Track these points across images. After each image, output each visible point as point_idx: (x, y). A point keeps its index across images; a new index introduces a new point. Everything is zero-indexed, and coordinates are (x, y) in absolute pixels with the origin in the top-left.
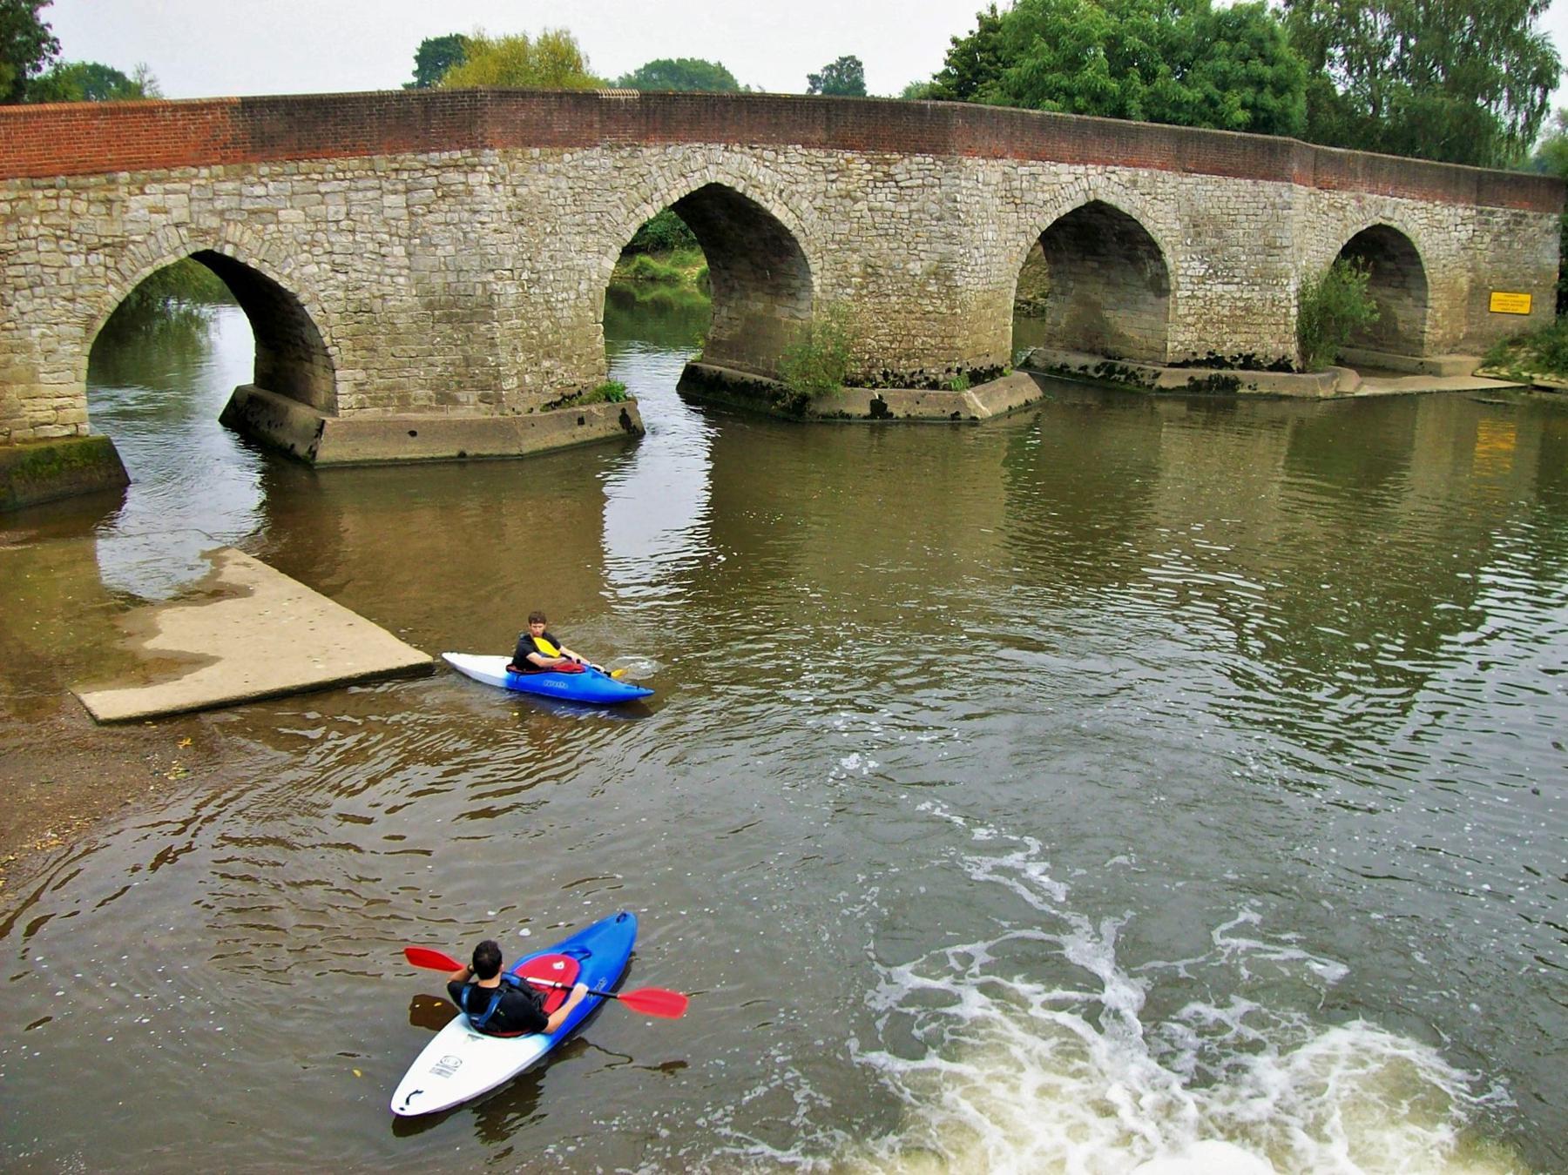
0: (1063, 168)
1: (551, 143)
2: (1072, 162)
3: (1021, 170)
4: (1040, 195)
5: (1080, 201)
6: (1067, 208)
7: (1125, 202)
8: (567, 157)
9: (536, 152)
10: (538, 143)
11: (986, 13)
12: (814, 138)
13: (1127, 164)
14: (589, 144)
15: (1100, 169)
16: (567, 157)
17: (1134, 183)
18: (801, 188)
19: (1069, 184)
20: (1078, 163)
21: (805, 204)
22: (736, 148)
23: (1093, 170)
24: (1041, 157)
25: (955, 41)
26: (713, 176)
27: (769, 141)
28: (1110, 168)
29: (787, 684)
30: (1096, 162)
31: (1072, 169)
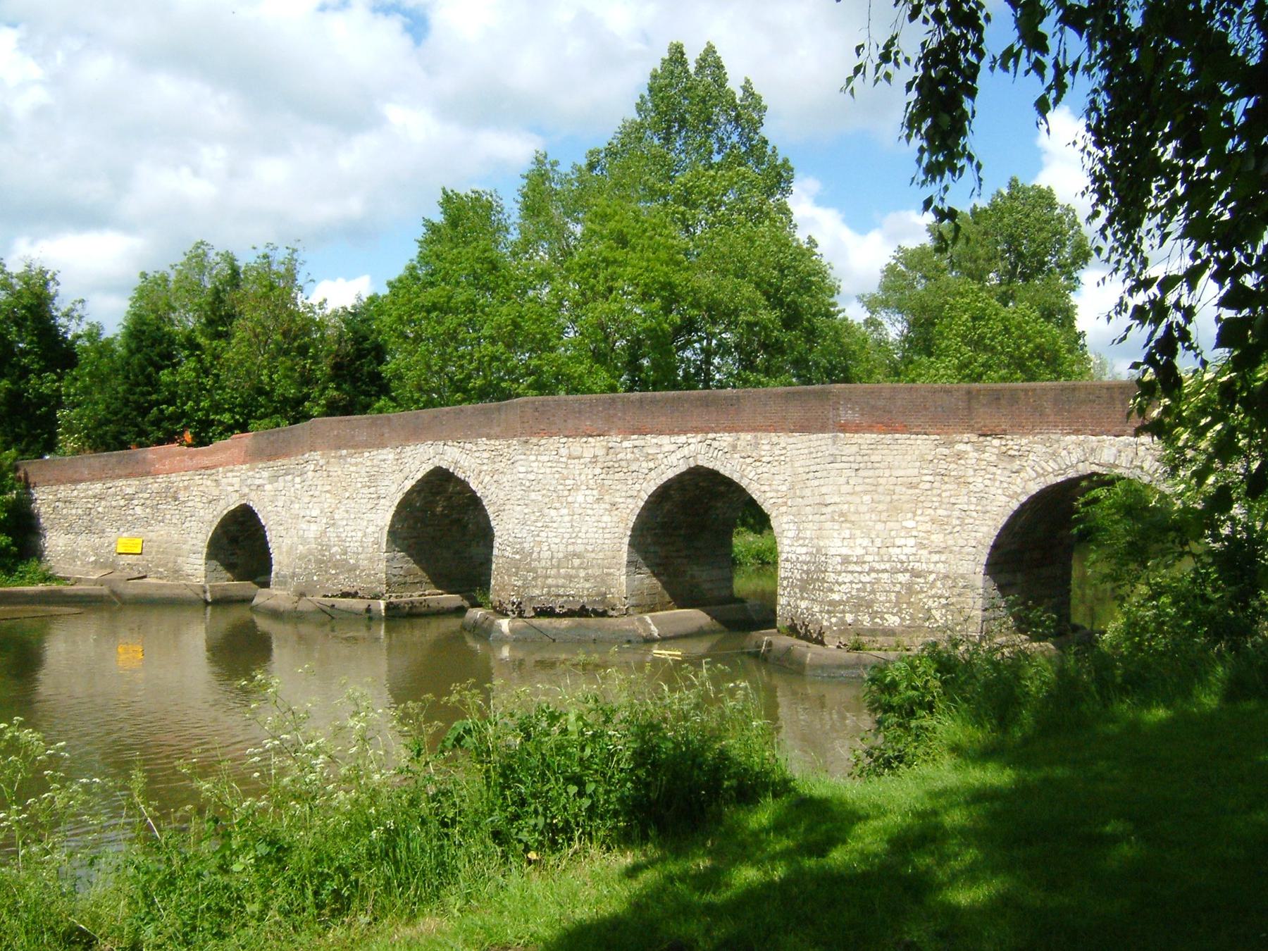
0: (664, 440)
1: (355, 447)
2: (671, 433)
3: (626, 444)
4: (644, 464)
5: (682, 468)
6: (670, 474)
7: (729, 468)
8: (366, 454)
9: (344, 452)
10: (346, 447)
11: (280, 255)
12: (492, 432)
13: (730, 430)
14: (382, 446)
15: (700, 437)
16: (366, 454)
17: (734, 447)
18: (485, 468)
19: (670, 454)
20: (678, 434)
21: (487, 478)
22: (450, 443)
23: (694, 439)
24: (642, 432)
25: (144, 275)
26: (437, 462)
27: (466, 436)
28: (711, 436)
29: (257, 759)
30: (696, 430)
31: (673, 439)
